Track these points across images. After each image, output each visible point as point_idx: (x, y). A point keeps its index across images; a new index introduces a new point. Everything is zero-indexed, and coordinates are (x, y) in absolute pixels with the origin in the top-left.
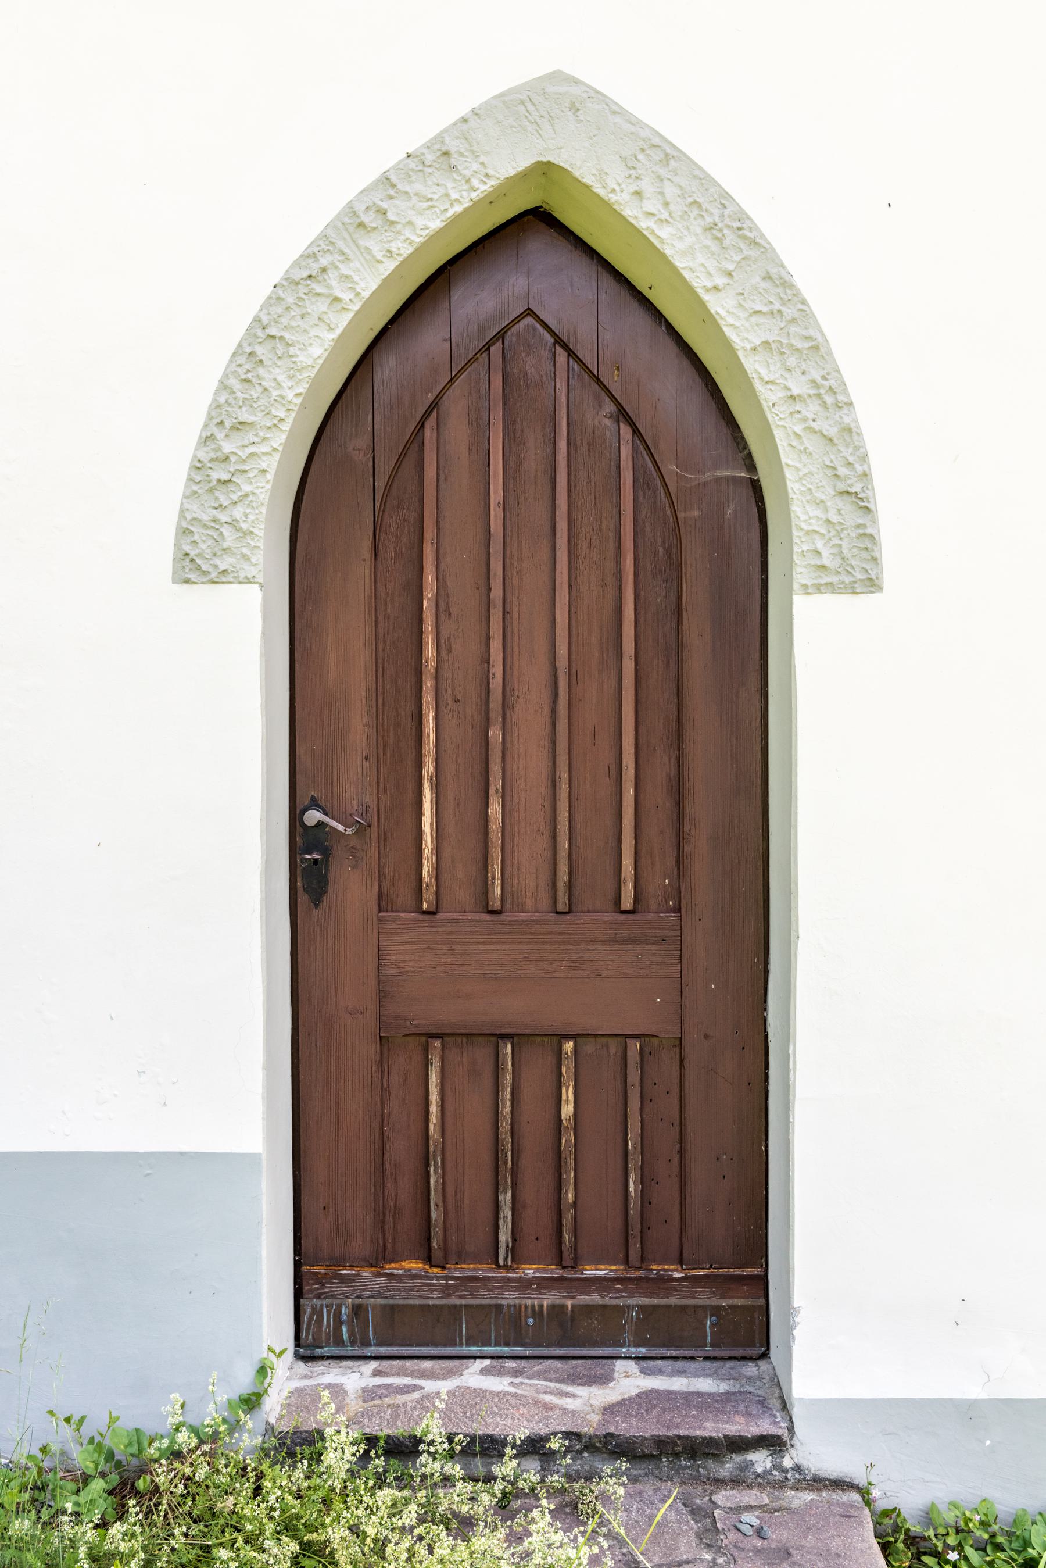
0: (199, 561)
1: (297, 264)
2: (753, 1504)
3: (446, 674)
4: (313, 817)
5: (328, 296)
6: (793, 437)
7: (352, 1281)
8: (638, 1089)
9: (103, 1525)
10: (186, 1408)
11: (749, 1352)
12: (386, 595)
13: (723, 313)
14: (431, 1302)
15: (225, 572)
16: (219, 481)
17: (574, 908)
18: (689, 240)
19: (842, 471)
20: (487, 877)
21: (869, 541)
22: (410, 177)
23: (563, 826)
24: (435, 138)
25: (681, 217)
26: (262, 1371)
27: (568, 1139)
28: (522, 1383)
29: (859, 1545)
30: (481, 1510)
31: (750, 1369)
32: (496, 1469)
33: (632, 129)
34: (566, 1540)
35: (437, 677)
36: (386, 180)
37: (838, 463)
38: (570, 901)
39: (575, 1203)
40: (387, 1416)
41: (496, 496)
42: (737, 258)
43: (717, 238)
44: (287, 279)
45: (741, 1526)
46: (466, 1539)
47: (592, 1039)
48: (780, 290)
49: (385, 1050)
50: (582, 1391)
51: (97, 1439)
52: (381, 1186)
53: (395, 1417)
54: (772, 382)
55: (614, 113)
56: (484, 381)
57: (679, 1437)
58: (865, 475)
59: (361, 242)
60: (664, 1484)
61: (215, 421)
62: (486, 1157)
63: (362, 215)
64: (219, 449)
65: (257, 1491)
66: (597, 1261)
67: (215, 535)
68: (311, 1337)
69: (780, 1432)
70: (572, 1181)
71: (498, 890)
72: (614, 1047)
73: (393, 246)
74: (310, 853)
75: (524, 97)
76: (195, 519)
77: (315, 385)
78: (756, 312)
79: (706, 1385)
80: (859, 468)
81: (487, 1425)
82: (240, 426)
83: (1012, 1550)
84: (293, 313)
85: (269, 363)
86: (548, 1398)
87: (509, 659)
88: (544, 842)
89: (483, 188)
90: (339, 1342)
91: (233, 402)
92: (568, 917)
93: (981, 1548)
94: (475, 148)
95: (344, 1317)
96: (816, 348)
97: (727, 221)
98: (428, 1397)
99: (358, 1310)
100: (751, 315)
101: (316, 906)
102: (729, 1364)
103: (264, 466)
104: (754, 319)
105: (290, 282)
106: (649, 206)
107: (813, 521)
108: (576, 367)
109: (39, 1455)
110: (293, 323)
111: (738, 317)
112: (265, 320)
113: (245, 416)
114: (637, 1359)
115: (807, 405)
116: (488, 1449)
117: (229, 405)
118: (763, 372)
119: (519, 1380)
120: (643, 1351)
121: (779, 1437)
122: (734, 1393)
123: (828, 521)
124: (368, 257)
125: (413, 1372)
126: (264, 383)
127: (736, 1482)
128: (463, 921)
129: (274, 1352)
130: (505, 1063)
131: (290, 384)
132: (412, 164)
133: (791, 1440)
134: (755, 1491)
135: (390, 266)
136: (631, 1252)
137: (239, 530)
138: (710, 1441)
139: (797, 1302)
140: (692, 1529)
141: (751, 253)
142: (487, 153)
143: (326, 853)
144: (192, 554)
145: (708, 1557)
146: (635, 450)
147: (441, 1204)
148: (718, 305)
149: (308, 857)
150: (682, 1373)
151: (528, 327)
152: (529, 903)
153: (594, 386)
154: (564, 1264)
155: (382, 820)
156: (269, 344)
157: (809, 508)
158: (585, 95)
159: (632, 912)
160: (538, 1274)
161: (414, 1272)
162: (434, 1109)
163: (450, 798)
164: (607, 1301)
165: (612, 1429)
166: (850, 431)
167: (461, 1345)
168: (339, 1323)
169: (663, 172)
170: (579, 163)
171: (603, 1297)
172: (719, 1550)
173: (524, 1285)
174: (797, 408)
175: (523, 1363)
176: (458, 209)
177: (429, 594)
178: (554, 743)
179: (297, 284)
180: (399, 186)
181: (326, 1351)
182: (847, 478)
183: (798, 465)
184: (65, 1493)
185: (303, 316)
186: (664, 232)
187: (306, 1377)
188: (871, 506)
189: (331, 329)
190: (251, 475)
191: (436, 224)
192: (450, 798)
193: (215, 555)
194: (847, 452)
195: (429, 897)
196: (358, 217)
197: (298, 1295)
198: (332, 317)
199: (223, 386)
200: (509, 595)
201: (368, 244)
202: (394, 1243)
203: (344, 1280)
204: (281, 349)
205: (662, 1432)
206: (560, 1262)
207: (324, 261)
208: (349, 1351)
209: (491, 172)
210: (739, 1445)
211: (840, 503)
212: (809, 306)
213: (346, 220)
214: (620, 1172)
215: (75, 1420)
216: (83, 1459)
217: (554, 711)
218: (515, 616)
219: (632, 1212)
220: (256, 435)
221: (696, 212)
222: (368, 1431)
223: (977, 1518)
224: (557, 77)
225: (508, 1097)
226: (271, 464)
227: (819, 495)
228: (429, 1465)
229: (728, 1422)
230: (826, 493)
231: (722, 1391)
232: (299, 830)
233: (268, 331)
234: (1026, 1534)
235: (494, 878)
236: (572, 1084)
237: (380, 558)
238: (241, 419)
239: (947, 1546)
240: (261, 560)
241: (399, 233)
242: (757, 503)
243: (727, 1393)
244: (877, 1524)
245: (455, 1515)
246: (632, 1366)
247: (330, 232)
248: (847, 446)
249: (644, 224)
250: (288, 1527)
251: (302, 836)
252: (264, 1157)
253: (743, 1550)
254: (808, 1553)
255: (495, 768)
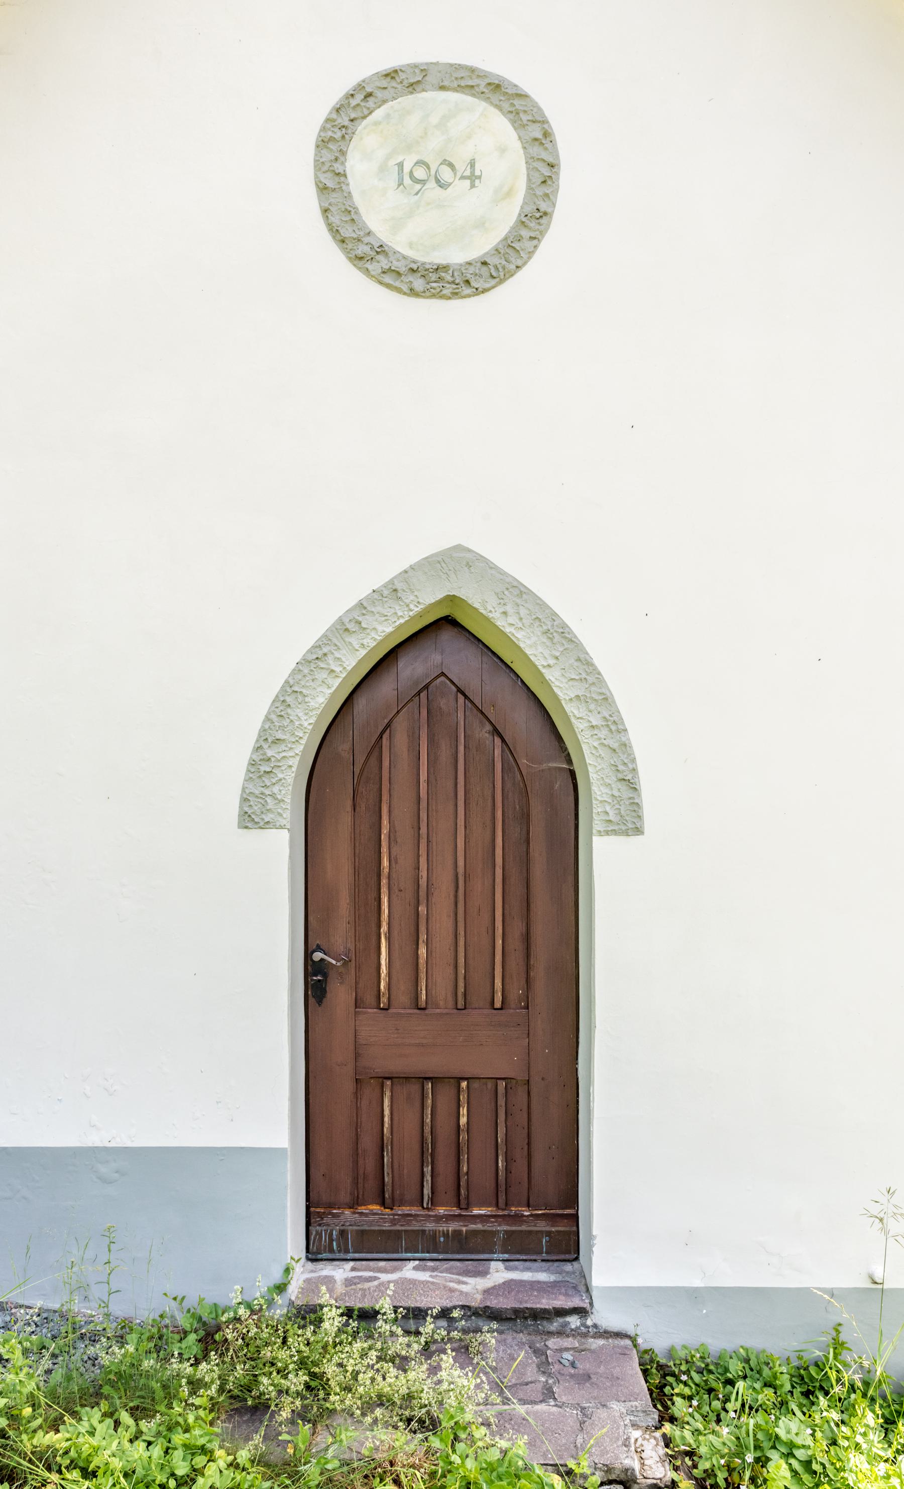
0: (253, 816)
1: (310, 651)
2: (570, 1347)
3: (394, 875)
4: (318, 956)
5: (327, 669)
6: (592, 748)
7: (339, 1216)
8: (504, 1108)
9: (197, 1362)
10: (244, 1291)
11: (567, 1257)
12: (360, 831)
13: (553, 679)
14: (384, 1228)
15: (268, 822)
16: (265, 772)
17: (467, 1006)
18: (534, 639)
19: (621, 768)
20: (417, 989)
21: (636, 807)
22: (374, 603)
23: (461, 961)
24: (389, 581)
25: (529, 626)
26: (287, 1270)
27: (463, 1136)
28: (437, 1276)
29: (630, 1372)
30: (413, 1353)
31: (568, 1267)
32: (421, 1329)
33: (502, 577)
34: (461, 1374)
35: (389, 877)
36: (361, 605)
37: (619, 764)
38: (465, 1003)
39: (467, 1172)
40: (359, 1295)
41: (423, 776)
42: (561, 649)
43: (550, 638)
44: (304, 660)
45: (563, 1361)
46: (405, 1371)
47: (478, 1080)
48: (585, 667)
49: (359, 1087)
50: (471, 1281)
51: (192, 1310)
52: (356, 1163)
53: (364, 1296)
54: (581, 718)
55: (491, 568)
56: (416, 711)
57: (527, 1308)
58: (634, 769)
59: (347, 639)
60: (518, 1335)
61: (263, 738)
62: (416, 1147)
63: (347, 624)
64: (265, 754)
65: (284, 1342)
66: (481, 1205)
67: (263, 802)
68: (315, 1248)
69: (585, 1306)
70: (466, 1160)
71: (424, 997)
72: (490, 1084)
73: (365, 642)
74: (316, 976)
75: (440, 559)
76: (251, 793)
77: (320, 717)
78: (572, 679)
79: (543, 1277)
80: (631, 766)
81: (416, 1301)
82: (277, 741)
83: (719, 1373)
84: (307, 679)
85: (294, 706)
86: (452, 1285)
87: (430, 867)
88: (450, 970)
89: (417, 609)
90: (331, 1250)
91: (273, 728)
92: (464, 1011)
93: (700, 1372)
94: (412, 587)
95: (335, 1237)
96: (606, 699)
97: (555, 628)
98: (382, 1284)
99: (343, 1233)
100: (569, 681)
101: (320, 1005)
102: (556, 1264)
103: (290, 763)
104: (571, 683)
105: (305, 661)
106: (511, 620)
107: (604, 795)
108: (470, 705)
109: (159, 1319)
110: (308, 684)
111: (562, 682)
112: (291, 682)
113: (280, 735)
114: (503, 1260)
115: (601, 731)
116: (417, 1315)
117: (271, 729)
118: (576, 712)
119: (435, 1273)
120: (506, 1256)
121: (584, 1309)
122: (559, 1282)
123: (613, 795)
124: (350, 647)
125: (374, 1268)
126: (291, 717)
127: (560, 1333)
128: (404, 1014)
129: (294, 1260)
130: (428, 1094)
131: (306, 718)
132: (376, 596)
133: (591, 1309)
134: (570, 1339)
135: (363, 652)
136: (500, 1200)
137: (277, 799)
138: (545, 1311)
139: (594, 1233)
140: (534, 1362)
141: (569, 646)
142: (419, 590)
143: (325, 975)
144: (249, 812)
145: (543, 1379)
146: (503, 751)
147: (390, 1173)
148: (548, 675)
149: (315, 978)
150: (528, 1269)
151: (442, 683)
152: (442, 1003)
153: (479, 715)
154: (461, 1207)
155: (357, 959)
156: (294, 696)
157: (602, 788)
158: (475, 558)
159: (501, 1009)
160: (446, 1213)
161: (375, 1211)
162: (387, 1119)
163: (397, 945)
164: (486, 1228)
165: (488, 1304)
166: (625, 745)
167: (402, 1252)
168: (331, 1240)
169: (519, 601)
170: (471, 596)
171: (483, 1226)
172: (550, 1375)
173: (439, 1219)
174: (595, 732)
175: (438, 1263)
176: (402, 621)
177: (385, 831)
178: (456, 914)
179: (310, 662)
180: (368, 608)
181: (324, 1256)
182: (623, 771)
183: (596, 764)
184: (173, 1341)
185: (313, 680)
186: (520, 635)
187: (312, 1271)
188: (637, 787)
189: (329, 687)
190: (283, 768)
191: (389, 629)
192: (397, 945)
193: (262, 813)
194: (623, 757)
195: (384, 1000)
196: (345, 625)
197: (308, 1224)
198: (330, 681)
199: (267, 719)
200: (430, 832)
201: (350, 640)
202: (363, 1195)
203: (335, 1216)
204: (300, 698)
205: (517, 1305)
206: (458, 1205)
207: (325, 650)
208: (337, 1256)
209: (421, 601)
210: (561, 1313)
211: (619, 785)
212: (602, 675)
213: (338, 627)
214: (493, 1154)
215: (179, 1299)
216: (184, 1322)
217: (456, 896)
218: (434, 844)
219: (500, 1178)
220: (286, 746)
221: (537, 623)
222: (348, 1304)
223: (698, 1355)
224: (459, 548)
225: (429, 1112)
226: (295, 762)
227: (608, 781)
228: (383, 1326)
229: (555, 1300)
230: (612, 780)
231: (552, 1280)
232: (310, 962)
233: (293, 689)
234: (726, 1364)
235: (421, 990)
236: (466, 1105)
237: (356, 811)
238: (278, 737)
239: (680, 1371)
240: (289, 816)
241: (368, 634)
242: (572, 780)
243: (555, 1282)
244: (640, 1358)
245: (398, 1356)
246: (500, 1265)
247: (328, 633)
248: (624, 753)
249: (508, 630)
250: (302, 1363)
251: (311, 966)
252: (289, 1150)
253: (563, 1375)
254: (601, 1376)
255: (423, 928)
